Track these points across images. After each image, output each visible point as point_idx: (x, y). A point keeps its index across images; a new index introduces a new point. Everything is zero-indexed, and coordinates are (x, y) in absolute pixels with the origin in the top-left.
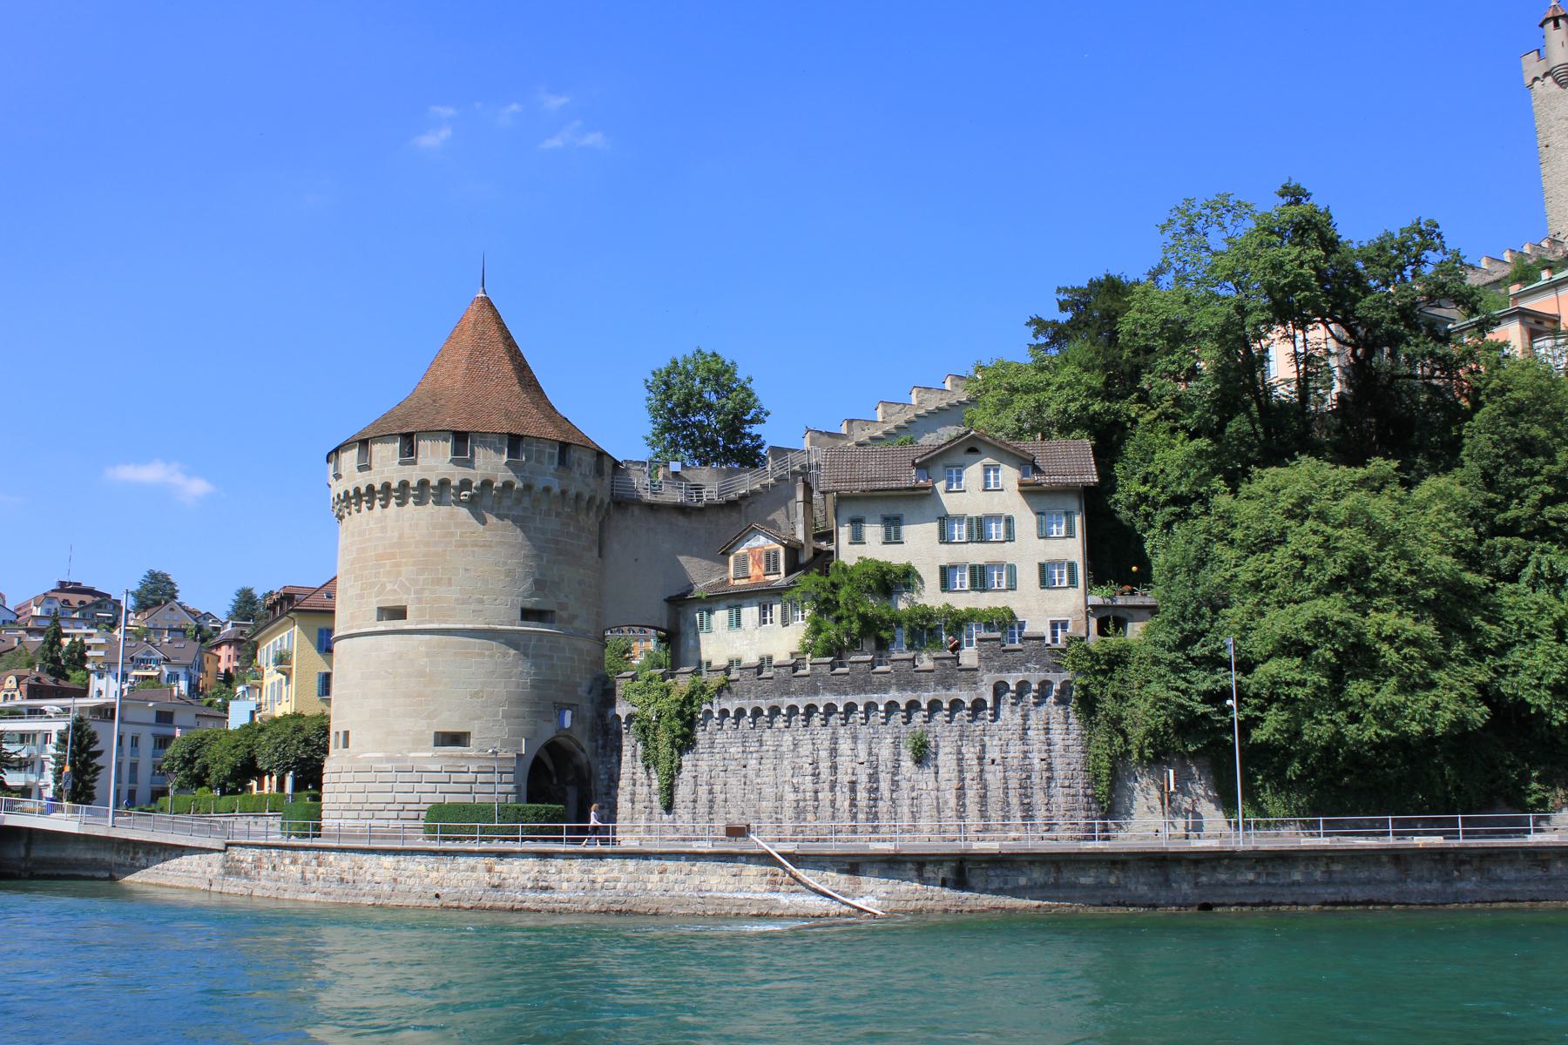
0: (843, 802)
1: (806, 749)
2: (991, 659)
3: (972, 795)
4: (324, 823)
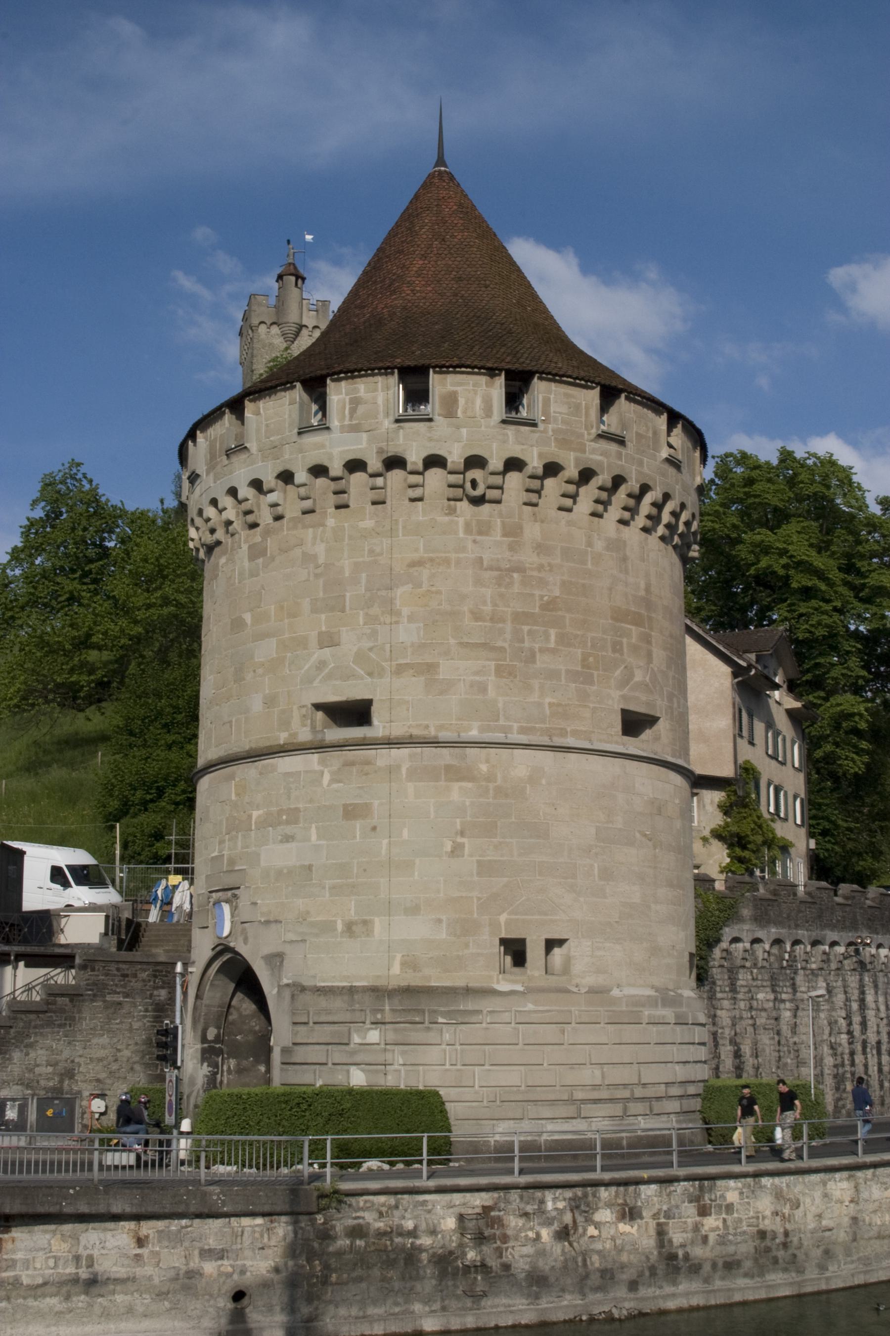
1: (840, 998)
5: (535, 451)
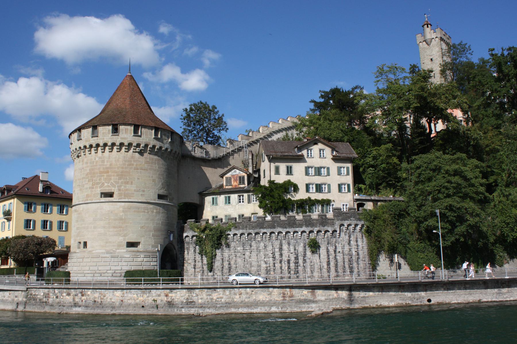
0: (285, 267)
1: (270, 248)
2: (339, 216)
3: (332, 264)
4: (71, 279)
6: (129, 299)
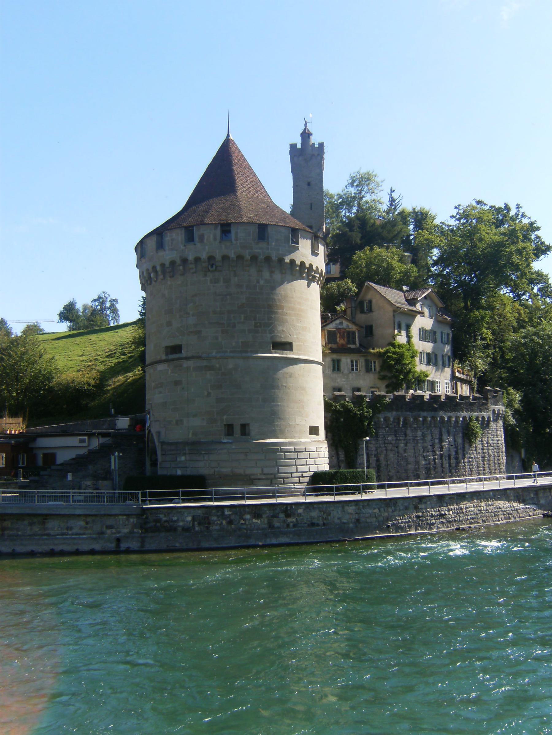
1: (429, 438)
5: (233, 252)
6: (368, 517)
